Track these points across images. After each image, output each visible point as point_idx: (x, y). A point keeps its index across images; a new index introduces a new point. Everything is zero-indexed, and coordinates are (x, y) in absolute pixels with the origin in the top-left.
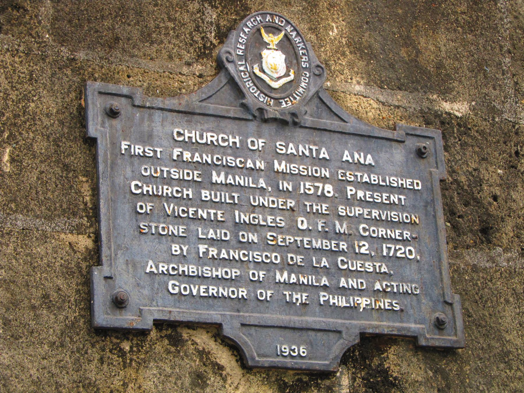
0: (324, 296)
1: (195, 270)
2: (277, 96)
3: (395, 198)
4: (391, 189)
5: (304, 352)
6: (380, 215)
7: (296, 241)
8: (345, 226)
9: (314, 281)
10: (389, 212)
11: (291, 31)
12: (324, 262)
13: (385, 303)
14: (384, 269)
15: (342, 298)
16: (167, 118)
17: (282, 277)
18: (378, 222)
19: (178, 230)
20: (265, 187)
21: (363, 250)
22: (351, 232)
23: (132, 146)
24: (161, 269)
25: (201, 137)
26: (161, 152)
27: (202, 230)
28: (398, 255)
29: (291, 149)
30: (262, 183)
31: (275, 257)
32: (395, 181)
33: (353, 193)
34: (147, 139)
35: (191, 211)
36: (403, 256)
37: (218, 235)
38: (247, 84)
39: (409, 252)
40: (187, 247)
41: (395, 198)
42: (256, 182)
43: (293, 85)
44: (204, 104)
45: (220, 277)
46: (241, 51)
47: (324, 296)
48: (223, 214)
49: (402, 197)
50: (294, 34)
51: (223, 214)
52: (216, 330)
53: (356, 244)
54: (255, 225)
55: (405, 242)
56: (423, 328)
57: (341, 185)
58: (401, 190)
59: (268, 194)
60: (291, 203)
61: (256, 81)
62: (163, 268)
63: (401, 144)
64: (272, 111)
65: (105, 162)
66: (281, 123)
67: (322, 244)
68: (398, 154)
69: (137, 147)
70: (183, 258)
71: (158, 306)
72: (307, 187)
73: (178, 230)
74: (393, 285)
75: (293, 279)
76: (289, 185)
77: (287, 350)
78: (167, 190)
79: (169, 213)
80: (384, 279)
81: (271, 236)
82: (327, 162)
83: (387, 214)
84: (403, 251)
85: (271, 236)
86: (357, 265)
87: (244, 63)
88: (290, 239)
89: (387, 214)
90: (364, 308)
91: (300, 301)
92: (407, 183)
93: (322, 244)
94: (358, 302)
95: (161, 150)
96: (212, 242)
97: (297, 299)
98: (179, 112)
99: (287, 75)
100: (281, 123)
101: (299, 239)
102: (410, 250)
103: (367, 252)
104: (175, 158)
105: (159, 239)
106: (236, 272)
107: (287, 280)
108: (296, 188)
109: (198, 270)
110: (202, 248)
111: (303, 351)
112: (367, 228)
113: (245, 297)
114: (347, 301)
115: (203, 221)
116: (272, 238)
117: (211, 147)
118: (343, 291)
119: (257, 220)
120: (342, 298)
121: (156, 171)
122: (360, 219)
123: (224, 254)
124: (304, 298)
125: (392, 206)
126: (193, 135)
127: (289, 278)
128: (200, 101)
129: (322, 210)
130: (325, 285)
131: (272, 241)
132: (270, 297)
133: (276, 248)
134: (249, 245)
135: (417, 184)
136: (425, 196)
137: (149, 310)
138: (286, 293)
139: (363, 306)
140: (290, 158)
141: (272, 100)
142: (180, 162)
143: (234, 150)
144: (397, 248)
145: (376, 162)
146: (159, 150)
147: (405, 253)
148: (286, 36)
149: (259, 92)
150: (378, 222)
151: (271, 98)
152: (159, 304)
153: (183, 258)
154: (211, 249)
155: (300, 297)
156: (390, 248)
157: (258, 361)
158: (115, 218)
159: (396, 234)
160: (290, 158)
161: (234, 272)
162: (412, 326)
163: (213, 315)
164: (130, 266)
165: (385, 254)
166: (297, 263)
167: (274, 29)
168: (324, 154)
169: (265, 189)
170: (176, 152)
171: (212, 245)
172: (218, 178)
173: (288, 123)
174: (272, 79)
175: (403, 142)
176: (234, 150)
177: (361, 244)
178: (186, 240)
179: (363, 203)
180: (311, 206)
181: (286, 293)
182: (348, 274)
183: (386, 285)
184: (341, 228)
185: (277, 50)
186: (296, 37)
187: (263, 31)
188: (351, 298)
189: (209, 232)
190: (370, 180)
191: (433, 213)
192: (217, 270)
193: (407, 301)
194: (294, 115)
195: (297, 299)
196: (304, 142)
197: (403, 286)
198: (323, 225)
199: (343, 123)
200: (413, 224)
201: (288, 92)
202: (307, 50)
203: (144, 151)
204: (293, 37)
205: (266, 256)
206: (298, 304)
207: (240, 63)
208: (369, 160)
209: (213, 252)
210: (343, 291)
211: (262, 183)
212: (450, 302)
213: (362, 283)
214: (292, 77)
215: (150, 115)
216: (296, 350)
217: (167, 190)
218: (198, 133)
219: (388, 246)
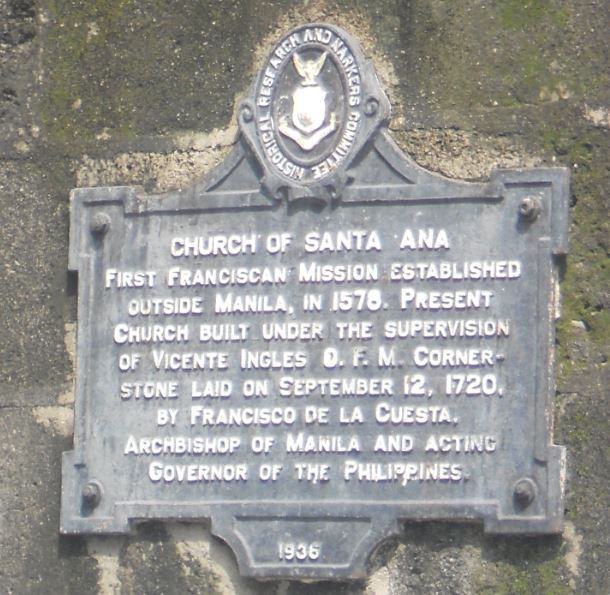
0: (351, 466)
1: (183, 444)
2: (305, 160)
3: (474, 298)
4: (471, 283)
5: (315, 553)
6: (447, 329)
7: (320, 385)
8: (392, 353)
9: (339, 445)
10: (462, 322)
11: (301, 37)
12: (358, 414)
13: (438, 471)
14: (445, 415)
15: (376, 467)
16: (166, 224)
17: (293, 443)
18: (442, 341)
19: (166, 388)
20: (284, 309)
21: (417, 390)
22: (402, 362)
23: (120, 274)
24: (142, 446)
25: (461, 270)
26: (154, 276)
27: (198, 385)
28: (470, 390)
29: (327, 242)
30: (281, 303)
31: (289, 414)
32: (476, 268)
33: (410, 298)
34: (140, 260)
35: (185, 357)
36: (478, 391)
37: (217, 391)
38: (269, 151)
39: (487, 384)
40: (176, 411)
41: (474, 298)
42: (271, 302)
43: (335, 136)
44: (212, 193)
45: (214, 451)
46: (265, 99)
47: (351, 466)
48: (226, 357)
49: (487, 294)
50: (343, 52)
51: (226, 357)
52: (198, 525)
53: (406, 380)
54: (267, 369)
55: (482, 367)
56: (495, 506)
57: (390, 286)
58: (487, 282)
59: (288, 318)
60: (318, 328)
61: (283, 143)
62: (145, 445)
63: (494, 208)
64: (301, 189)
65: (87, 303)
66: (316, 205)
67: (356, 386)
68: (493, 221)
69: (125, 274)
70: (170, 429)
71: (136, 498)
72: (343, 299)
73: (166, 388)
74: (454, 441)
75: (310, 445)
76: (317, 300)
77: (292, 552)
78: (159, 332)
79: (158, 365)
80: (443, 432)
81: (286, 382)
82: (380, 254)
83: (459, 324)
84: (477, 383)
85: (286, 382)
86: (402, 414)
87: (267, 118)
88: (311, 383)
89: (459, 324)
90: (409, 481)
91: (316, 478)
92: (495, 268)
93: (356, 386)
94: (399, 472)
95: (154, 273)
96: (209, 400)
97: (313, 475)
98: (181, 212)
99: (325, 124)
100: (316, 205)
101: (323, 382)
102: (490, 381)
103: (422, 391)
104: (171, 282)
105: (145, 404)
106: (235, 442)
107: (301, 447)
108: (327, 302)
109: (187, 443)
110: (195, 410)
111: (312, 551)
112: (426, 352)
113: (244, 478)
114: (385, 471)
115: (200, 372)
116: (286, 386)
117: (215, 259)
118: (383, 457)
119: (268, 361)
120: (376, 467)
121: (146, 307)
122: (417, 339)
123: (222, 418)
124: (323, 471)
125: (469, 311)
126: (194, 245)
127: (305, 442)
128: (208, 191)
129: (361, 332)
130: (354, 450)
131: (287, 389)
132: (278, 474)
133: (290, 399)
134: (256, 400)
135: (514, 267)
136: (526, 284)
137: (124, 506)
138: (298, 466)
139: (406, 477)
140: (325, 256)
141: (303, 170)
142: (177, 290)
143: (250, 258)
144: (469, 380)
145: (453, 240)
146: (151, 274)
147: (480, 385)
148: (330, 57)
149: (285, 160)
150: (442, 341)
151: (300, 165)
152: (139, 496)
153: (170, 429)
154: (205, 411)
155: (317, 471)
156: (457, 381)
157: (253, 569)
158: (94, 380)
159: (468, 356)
160: (325, 256)
161: (232, 442)
162: (478, 501)
163: (197, 505)
164: (107, 445)
165: (449, 391)
166: (317, 419)
167: (310, 52)
168: (375, 241)
169: (284, 312)
170: (172, 273)
171: (209, 405)
172: (222, 304)
173: (322, 204)
174: (304, 134)
175: (500, 199)
176: (250, 258)
177: (413, 380)
178: (178, 401)
179: (424, 312)
180: (346, 329)
181: (298, 466)
182: (388, 428)
183: (445, 441)
184: (385, 356)
185: (315, 85)
186: (346, 56)
187: (297, 57)
188: (390, 465)
189: (205, 386)
190: (439, 273)
191: (535, 314)
192: (211, 441)
193: (476, 463)
194: (330, 188)
195: (313, 475)
196: (344, 227)
197: (470, 439)
198: (362, 355)
199: (406, 185)
200: (501, 337)
201: (326, 152)
202: (360, 76)
203: (133, 281)
204: (342, 57)
205: (277, 414)
206: (315, 482)
207: (262, 119)
208: (443, 239)
209: (208, 415)
210: (383, 457)
211: (281, 303)
212: (542, 459)
213: (408, 441)
214: (331, 127)
215: (146, 224)
216: (304, 551)
217: (159, 332)
218: (201, 239)
219: (456, 377)
